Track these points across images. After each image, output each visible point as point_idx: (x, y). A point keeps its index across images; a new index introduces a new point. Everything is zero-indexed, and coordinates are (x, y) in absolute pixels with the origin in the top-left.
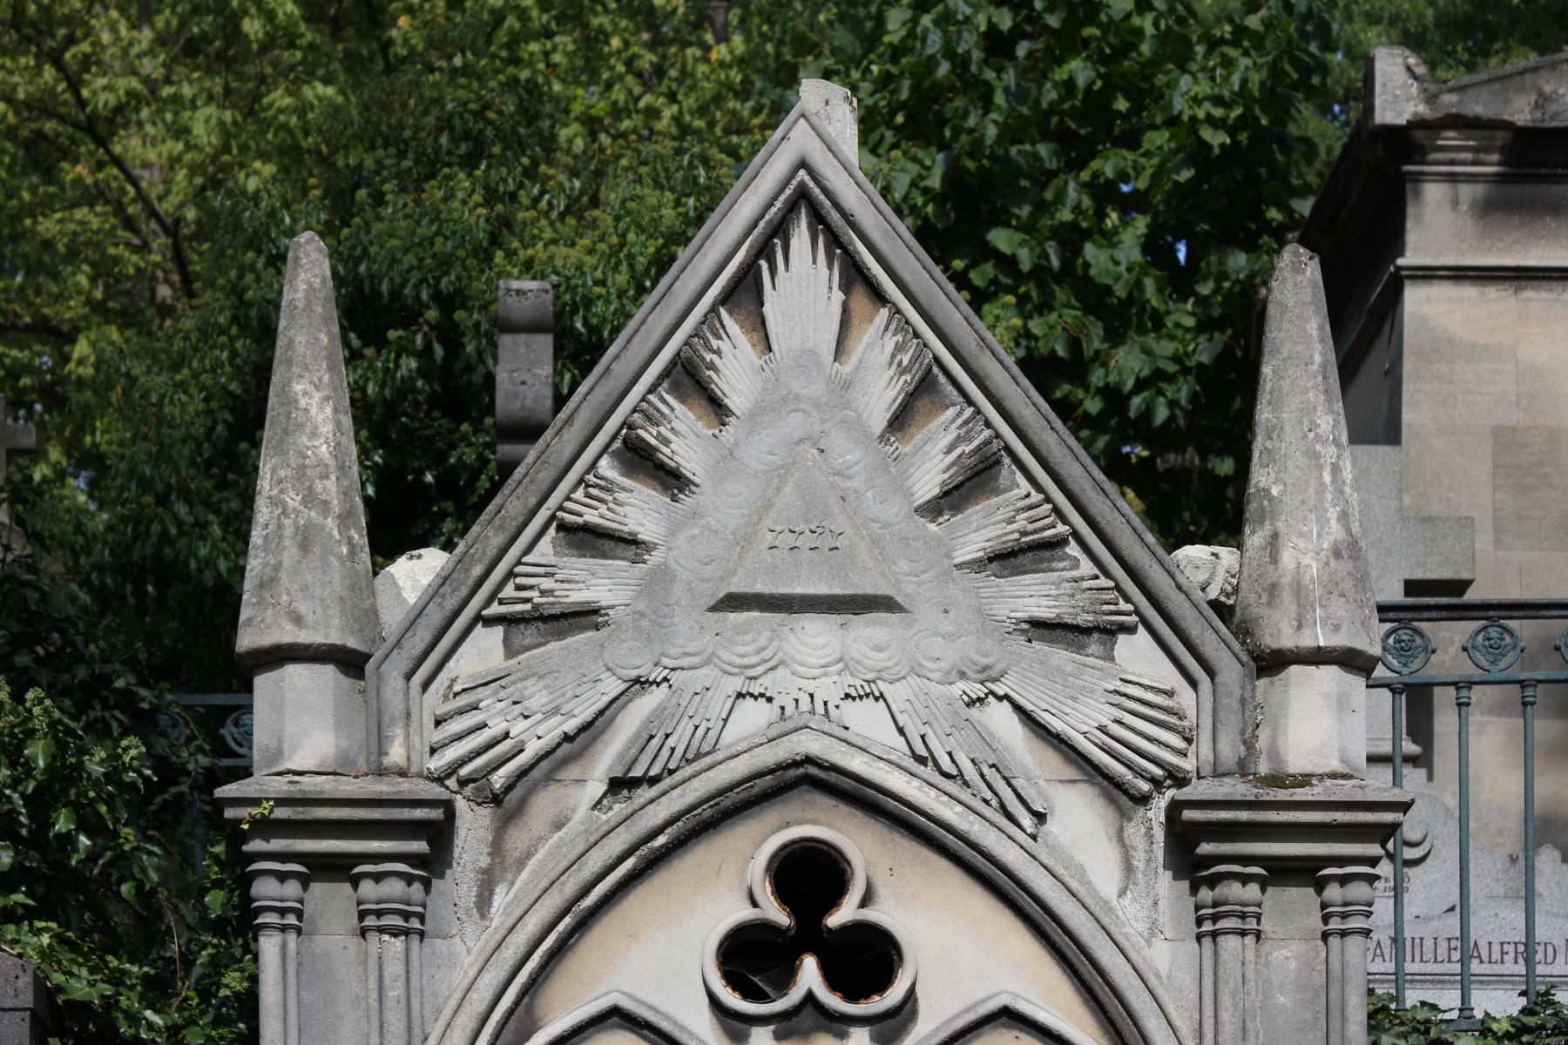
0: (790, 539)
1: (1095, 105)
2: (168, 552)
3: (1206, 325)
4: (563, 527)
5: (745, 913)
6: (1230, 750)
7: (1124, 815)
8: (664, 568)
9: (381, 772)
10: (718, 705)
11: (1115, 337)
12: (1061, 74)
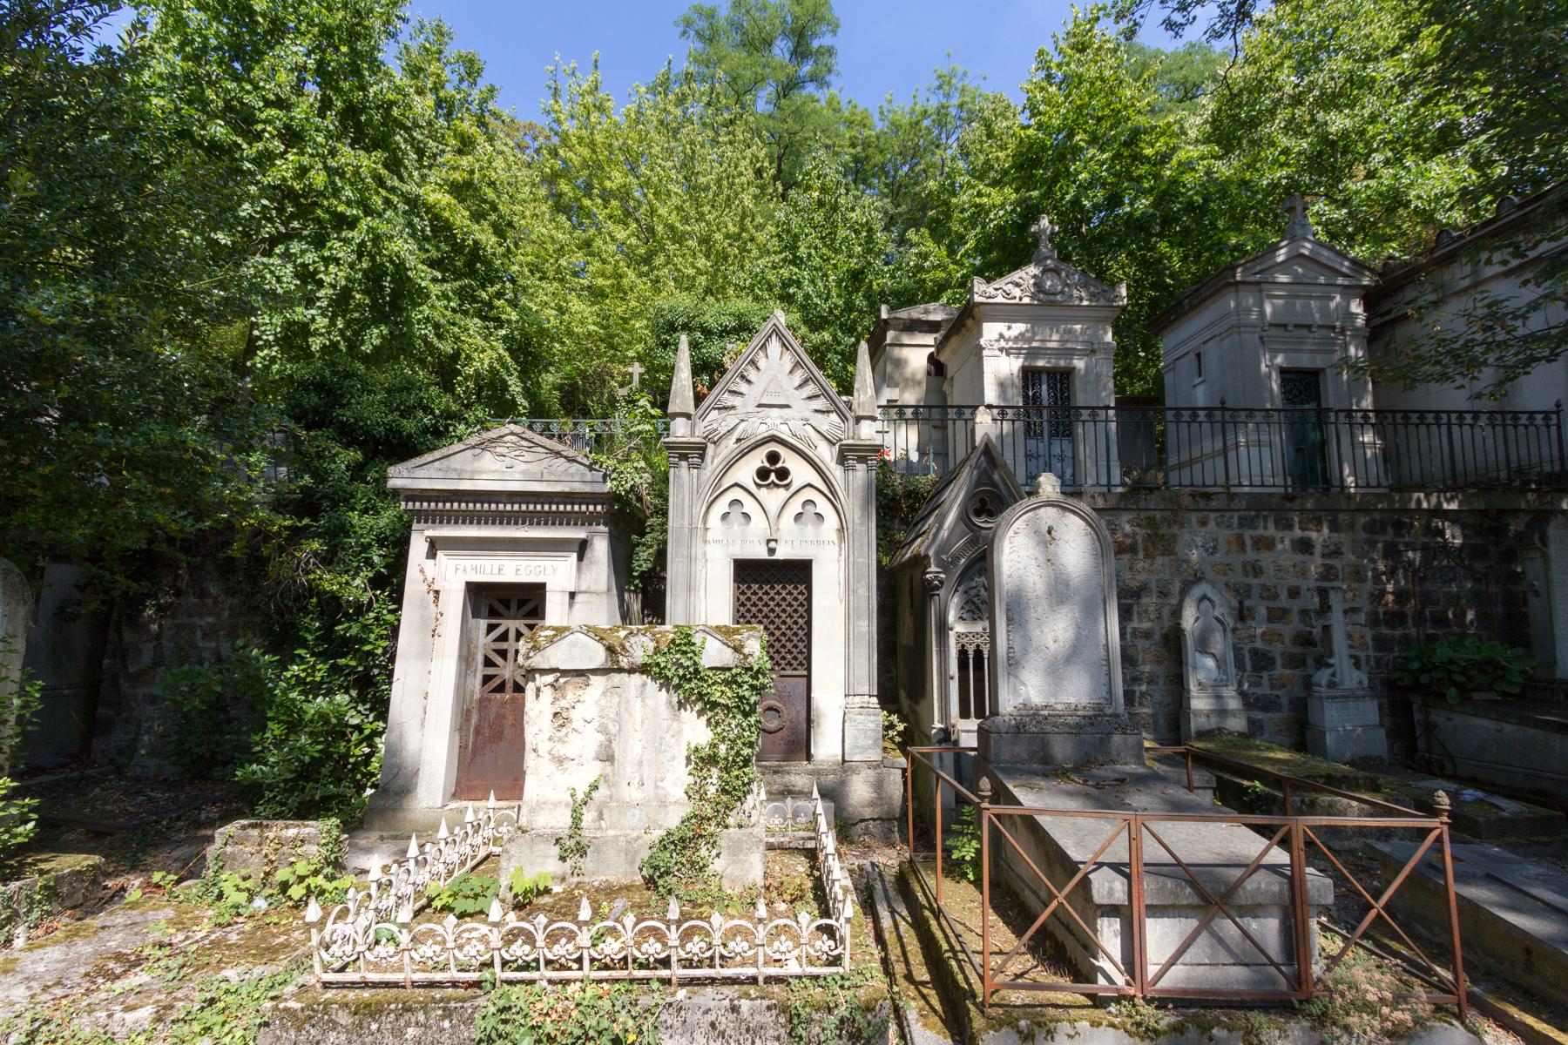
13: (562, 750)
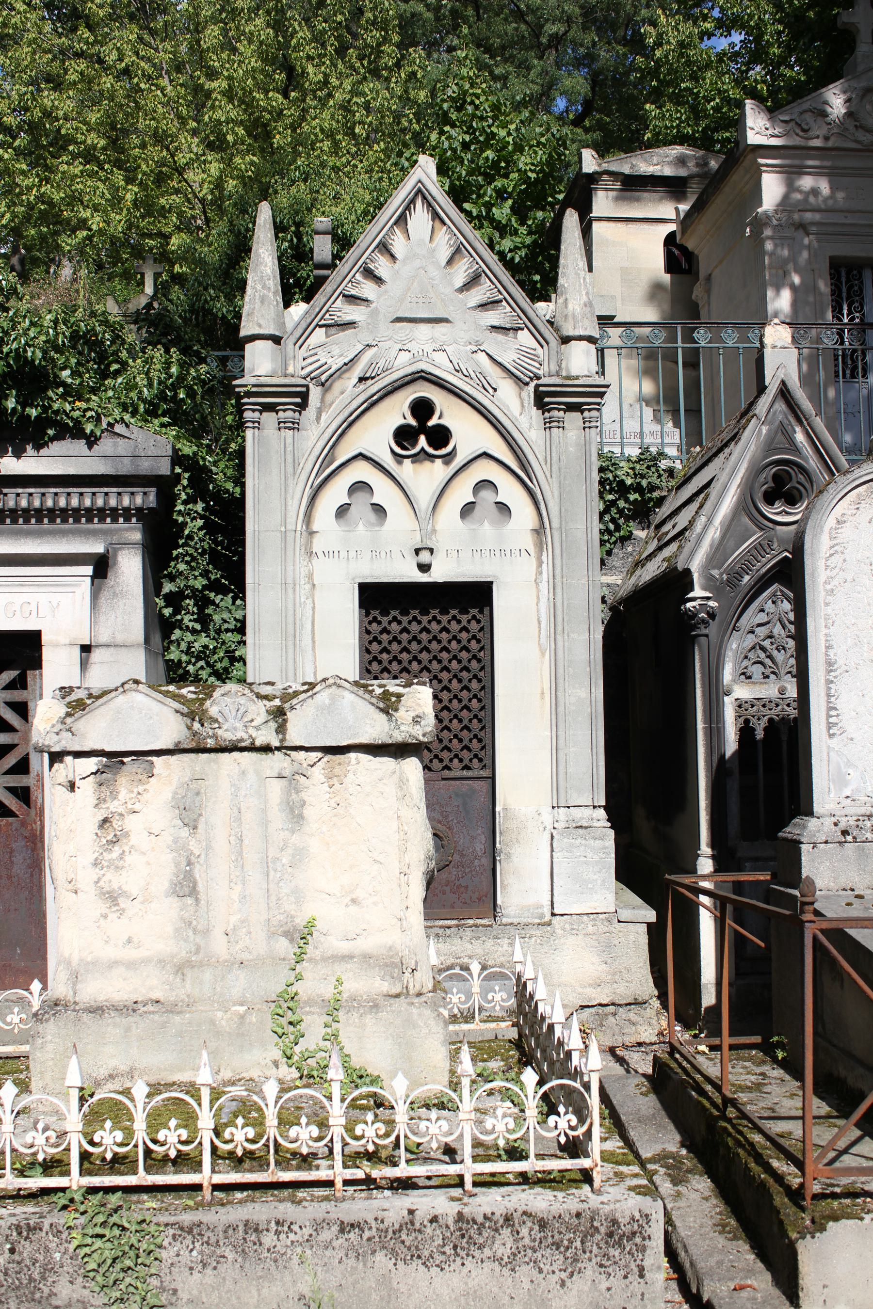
0: (416, 300)
1: (495, 164)
2: (207, 306)
3: (530, 233)
4: (344, 296)
5: (402, 422)
6: (554, 368)
7: (521, 389)
8: (376, 309)
9: (286, 376)
10: (394, 353)
11: (502, 237)
12: (484, 155)
13: (113, 880)
